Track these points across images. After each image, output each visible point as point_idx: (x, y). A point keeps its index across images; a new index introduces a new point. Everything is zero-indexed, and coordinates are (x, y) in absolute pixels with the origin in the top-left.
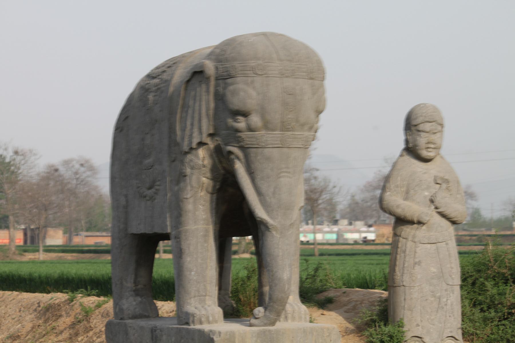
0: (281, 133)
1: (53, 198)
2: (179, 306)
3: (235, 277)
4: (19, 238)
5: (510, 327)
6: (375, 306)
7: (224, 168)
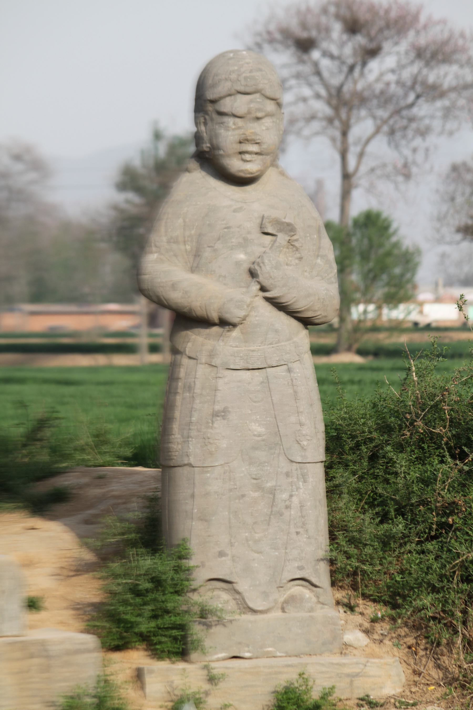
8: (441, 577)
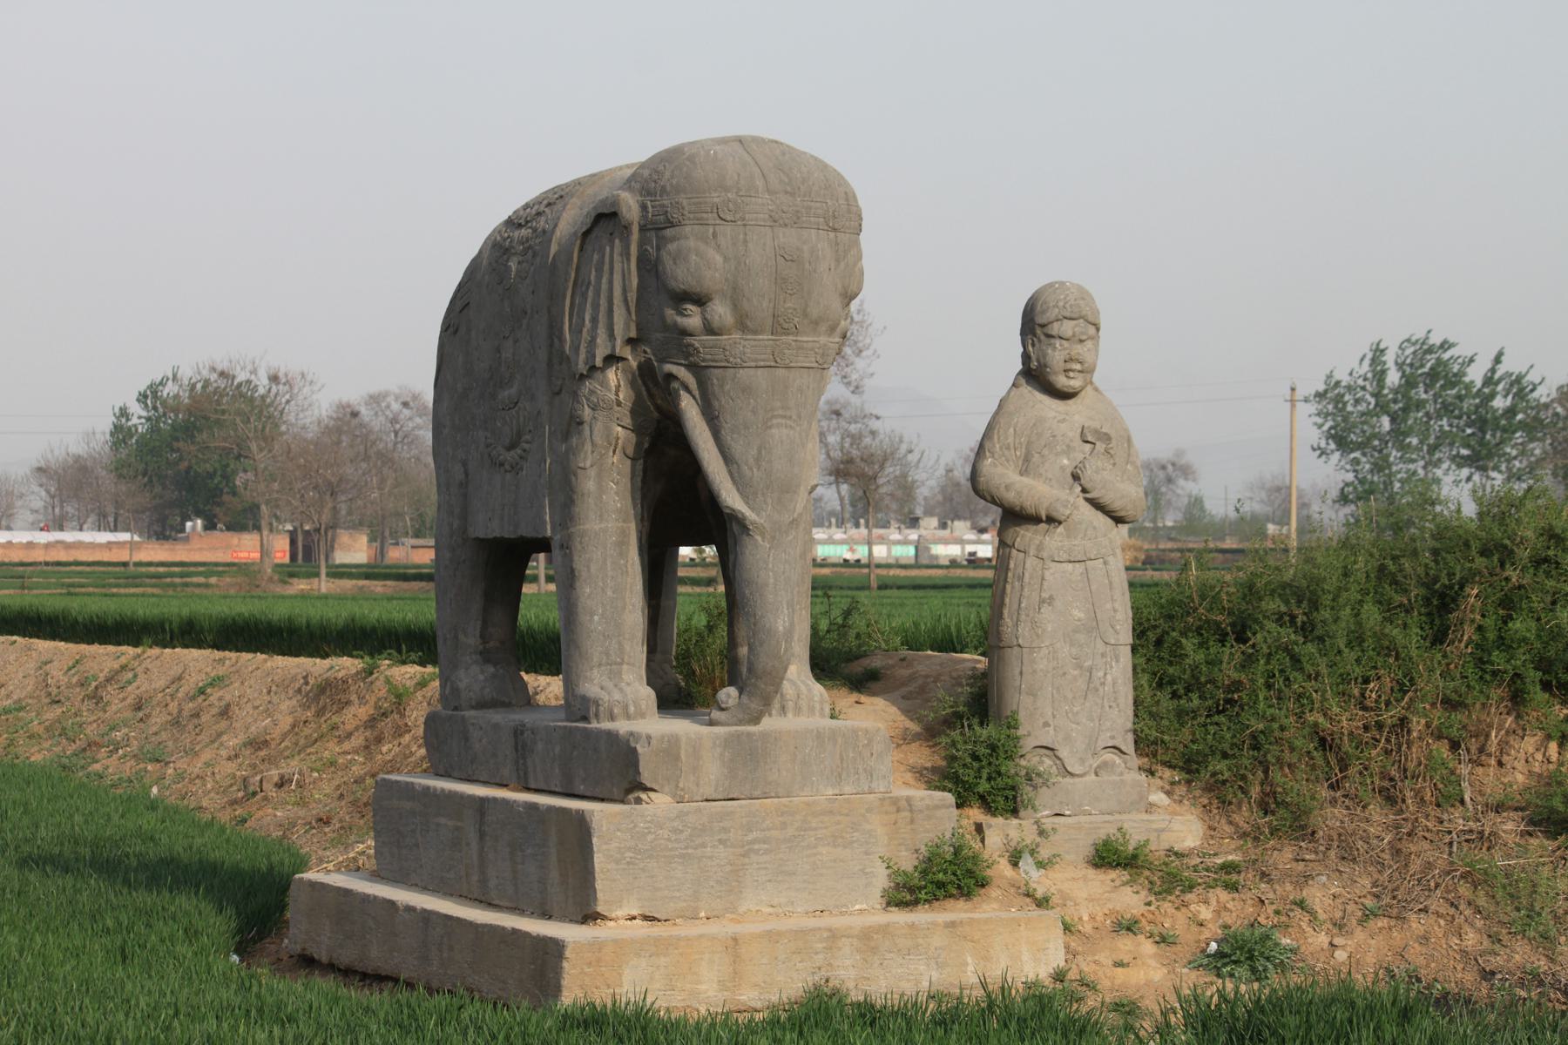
0: (773, 337)
1: (349, 470)
2: (569, 686)
3: (682, 627)
4: (280, 548)
5: (1229, 728)
6: (962, 686)
7: (658, 408)
8: (1233, 745)
